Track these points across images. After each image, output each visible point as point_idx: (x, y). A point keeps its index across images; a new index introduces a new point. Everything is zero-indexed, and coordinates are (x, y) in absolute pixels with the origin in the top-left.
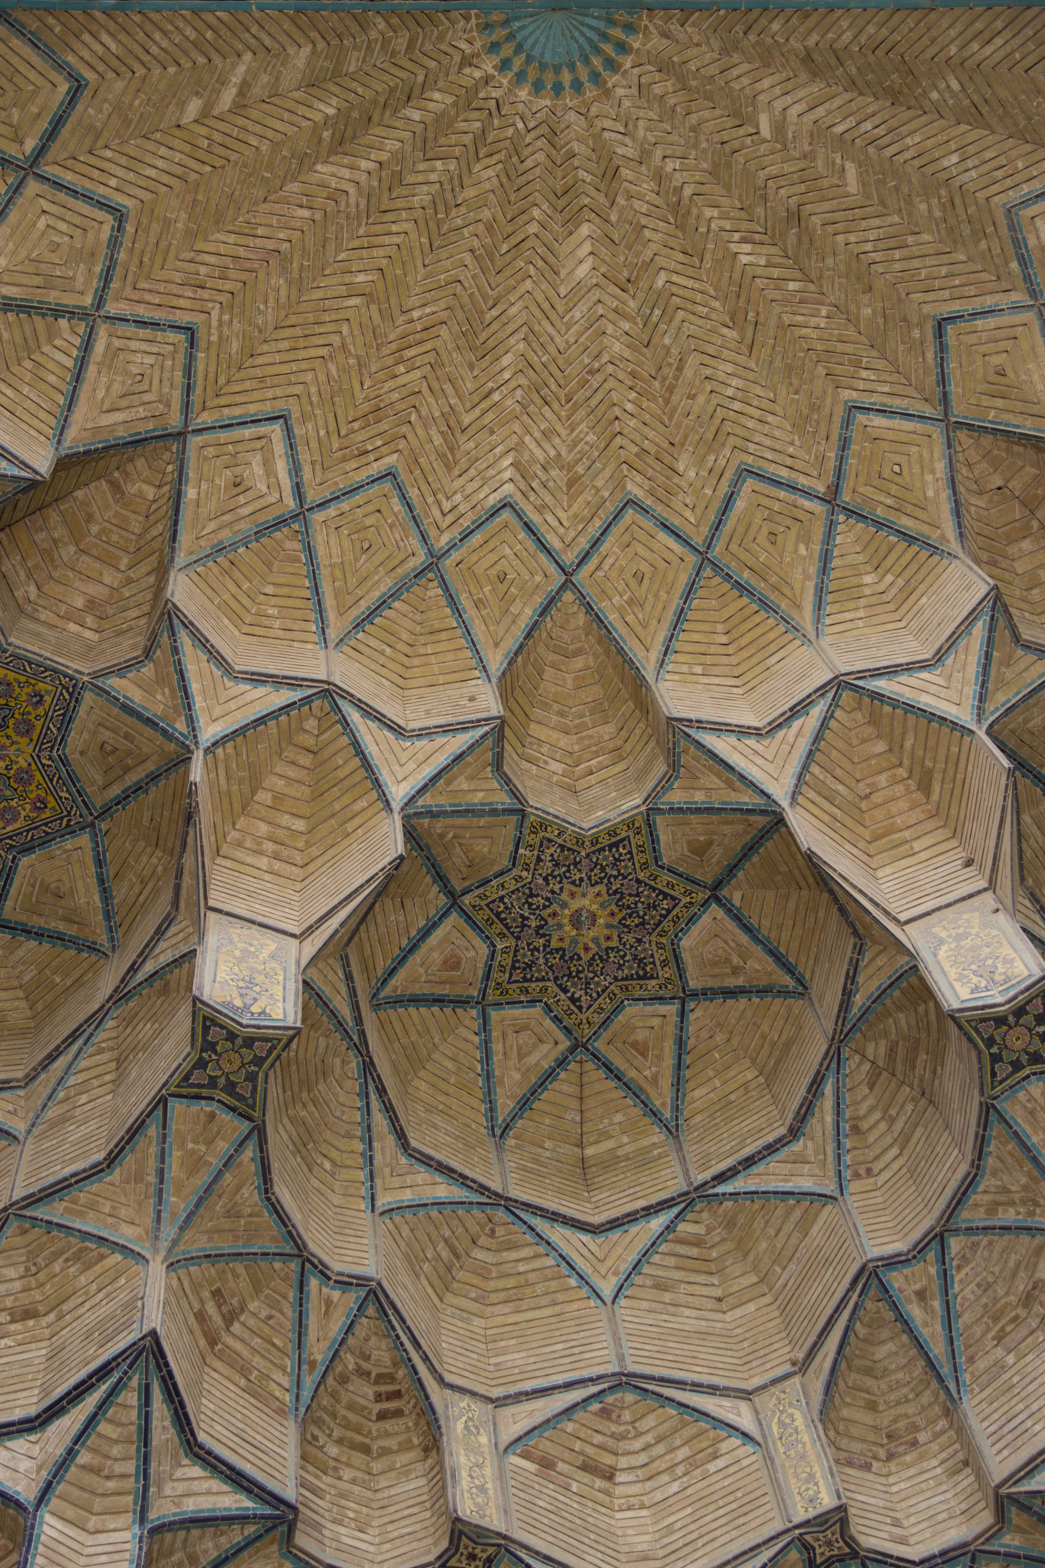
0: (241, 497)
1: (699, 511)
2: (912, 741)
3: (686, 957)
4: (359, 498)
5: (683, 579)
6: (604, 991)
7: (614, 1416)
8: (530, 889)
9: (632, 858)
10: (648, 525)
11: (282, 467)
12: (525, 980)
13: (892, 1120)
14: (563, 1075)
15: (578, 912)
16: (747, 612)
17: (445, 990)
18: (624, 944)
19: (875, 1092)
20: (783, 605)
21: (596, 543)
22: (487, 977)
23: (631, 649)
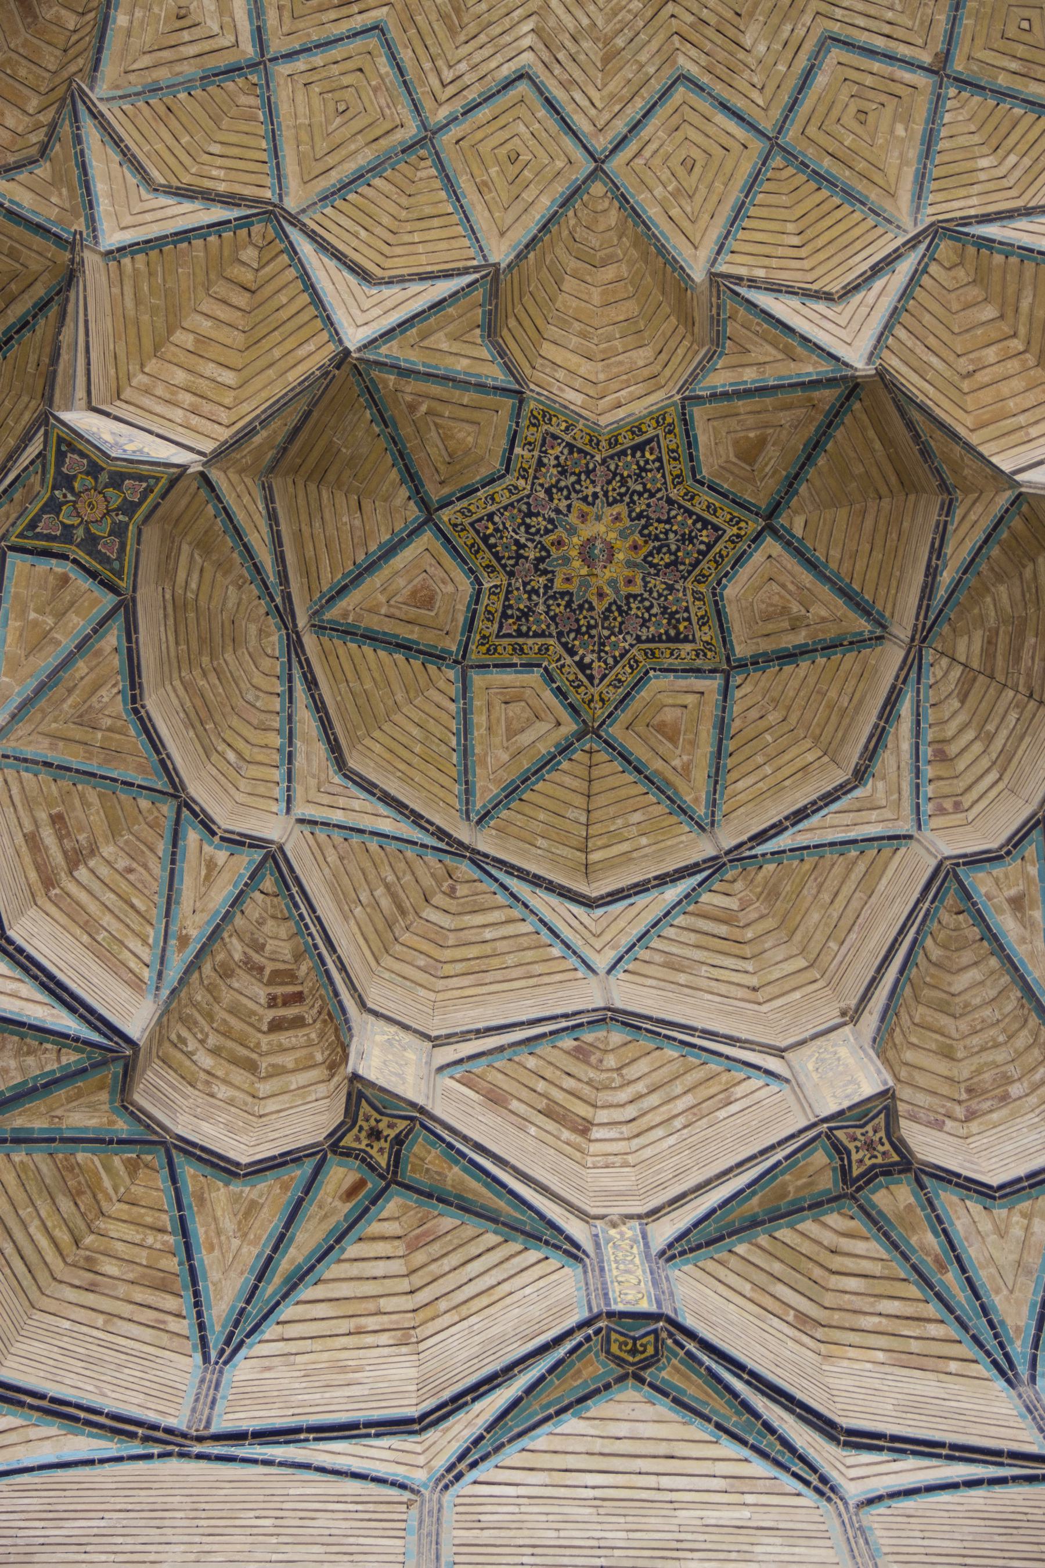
0: (185, 33)
1: (769, 91)
2: (1030, 300)
3: (732, 611)
4: (336, 53)
5: (746, 169)
6: (622, 656)
7: (593, 1059)
8: (528, 504)
9: (662, 467)
10: (704, 105)
12: (520, 634)
13: (991, 738)
14: (565, 765)
15: (590, 541)
16: (825, 207)
17: (413, 634)
18: (651, 592)
19: (967, 705)
20: (874, 195)
21: (636, 126)
23: (675, 248)
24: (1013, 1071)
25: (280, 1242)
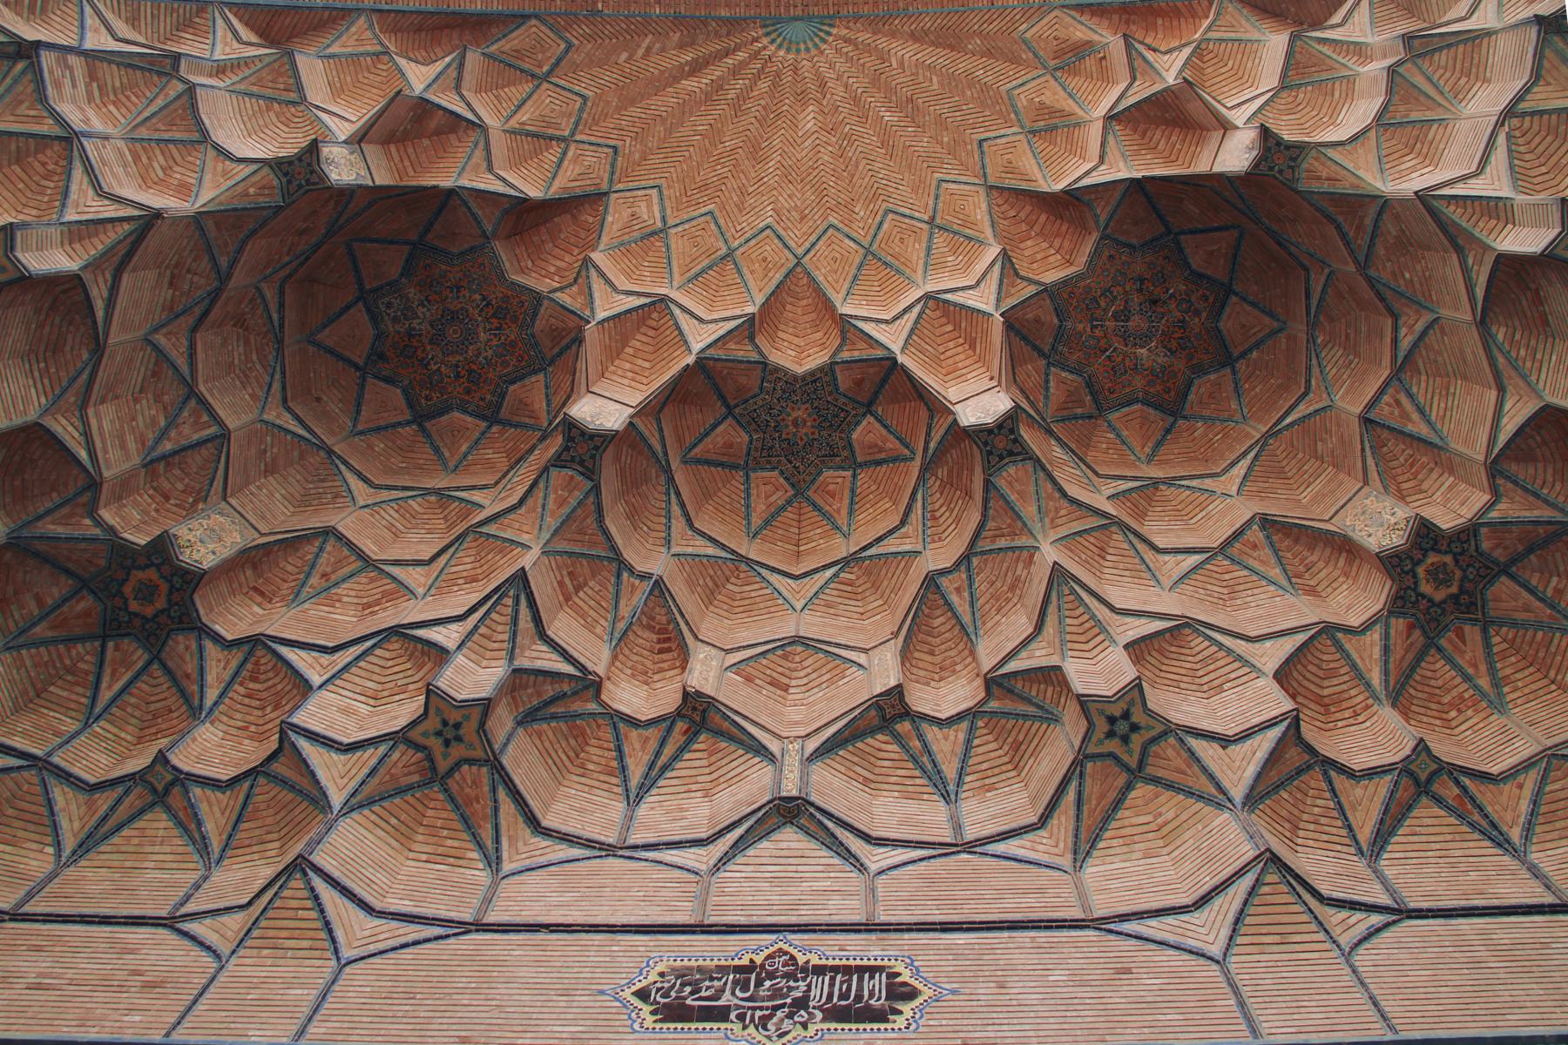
3: (855, 444)
4: (694, 223)
10: (840, 236)
11: (656, 209)
17: (724, 459)
21: (813, 245)
22: (748, 454)
24: (958, 659)
25: (658, 754)
